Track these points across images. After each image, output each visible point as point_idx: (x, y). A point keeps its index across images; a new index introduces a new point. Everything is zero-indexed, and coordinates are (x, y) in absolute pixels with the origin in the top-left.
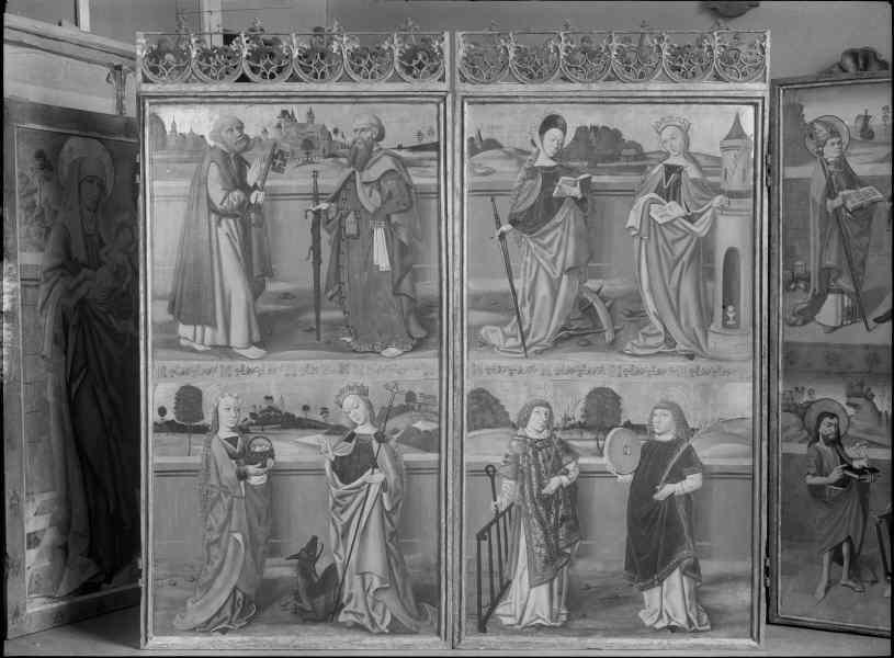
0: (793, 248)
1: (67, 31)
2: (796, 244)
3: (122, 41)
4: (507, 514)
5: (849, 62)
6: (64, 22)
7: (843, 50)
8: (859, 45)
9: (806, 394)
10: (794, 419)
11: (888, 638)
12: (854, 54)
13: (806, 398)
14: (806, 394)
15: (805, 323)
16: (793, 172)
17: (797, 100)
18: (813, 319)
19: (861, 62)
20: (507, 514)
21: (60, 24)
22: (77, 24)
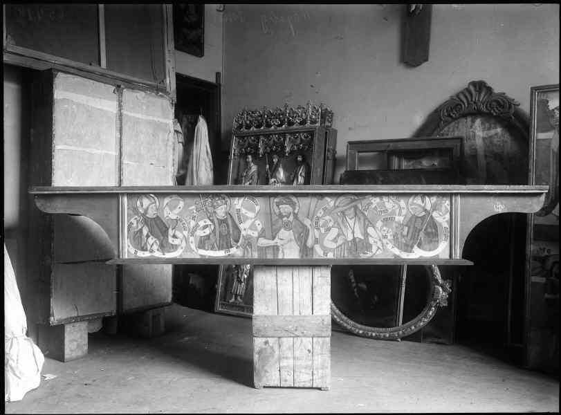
0: (541, 175)
1: (94, 68)
2: (543, 174)
3: (67, 58)
4: (343, 246)
5: (472, 88)
6: (93, 64)
7: (469, 82)
8: (477, 79)
9: (546, 252)
10: (538, 264)
11: (451, 255)
12: (474, 84)
13: (546, 253)
14: (546, 252)
15: (546, 215)
16: (542, 136)
17: (545, 98)
18: (551, 211)
19: (478, 88)
20: (343, 246)
21: (91, 64)
22: (100, 64)
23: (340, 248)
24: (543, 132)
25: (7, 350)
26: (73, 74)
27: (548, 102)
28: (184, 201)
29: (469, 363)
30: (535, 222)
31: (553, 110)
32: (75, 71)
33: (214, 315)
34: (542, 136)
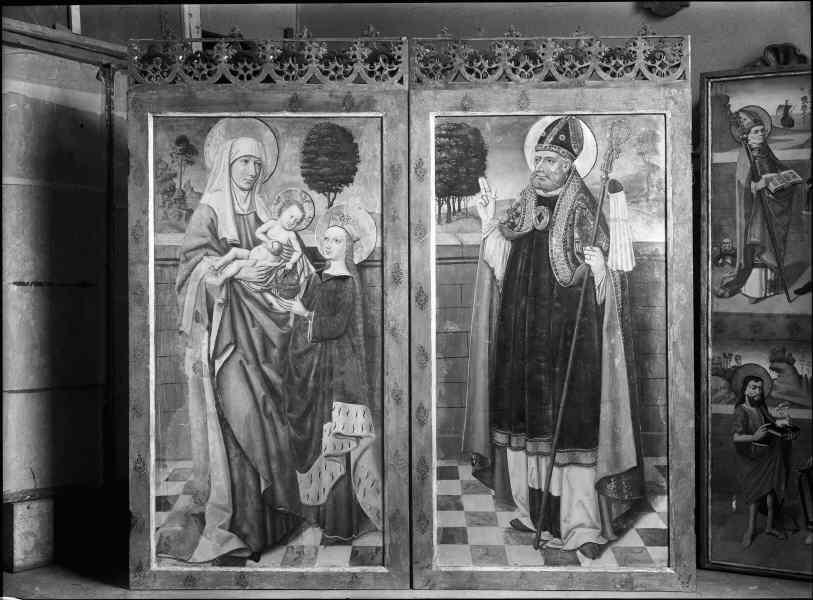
1: (60, 33)
2: (724, 222)
6: (57, 25)
9: (733, 360)
10: (722, 382)
13: (733, 363)
14: (733, 360)
16: (720, 158)
21: (54, 27)
22: (69, 27)
23: (279, 537)
24: (722, 150)
25: (810, 250)
26: (24, 47)
27: (728, 98)
28: (134, 264)
29: (28, 216)
30: (715, 310)
31: (737, 113)
32: (23, 41)
33: (747, 180)
34: (720, 158)
